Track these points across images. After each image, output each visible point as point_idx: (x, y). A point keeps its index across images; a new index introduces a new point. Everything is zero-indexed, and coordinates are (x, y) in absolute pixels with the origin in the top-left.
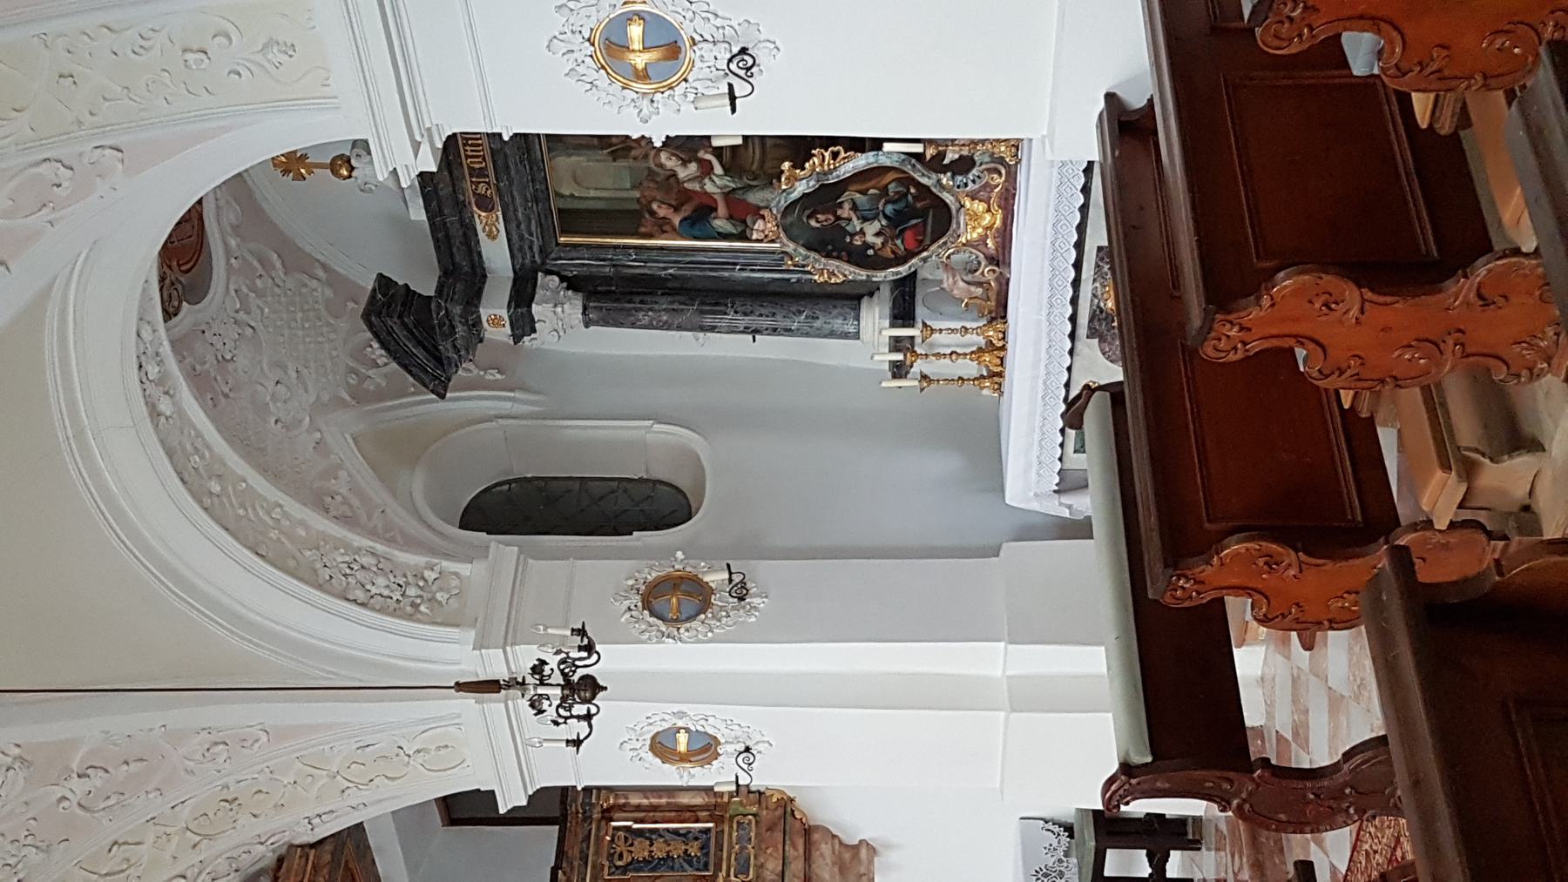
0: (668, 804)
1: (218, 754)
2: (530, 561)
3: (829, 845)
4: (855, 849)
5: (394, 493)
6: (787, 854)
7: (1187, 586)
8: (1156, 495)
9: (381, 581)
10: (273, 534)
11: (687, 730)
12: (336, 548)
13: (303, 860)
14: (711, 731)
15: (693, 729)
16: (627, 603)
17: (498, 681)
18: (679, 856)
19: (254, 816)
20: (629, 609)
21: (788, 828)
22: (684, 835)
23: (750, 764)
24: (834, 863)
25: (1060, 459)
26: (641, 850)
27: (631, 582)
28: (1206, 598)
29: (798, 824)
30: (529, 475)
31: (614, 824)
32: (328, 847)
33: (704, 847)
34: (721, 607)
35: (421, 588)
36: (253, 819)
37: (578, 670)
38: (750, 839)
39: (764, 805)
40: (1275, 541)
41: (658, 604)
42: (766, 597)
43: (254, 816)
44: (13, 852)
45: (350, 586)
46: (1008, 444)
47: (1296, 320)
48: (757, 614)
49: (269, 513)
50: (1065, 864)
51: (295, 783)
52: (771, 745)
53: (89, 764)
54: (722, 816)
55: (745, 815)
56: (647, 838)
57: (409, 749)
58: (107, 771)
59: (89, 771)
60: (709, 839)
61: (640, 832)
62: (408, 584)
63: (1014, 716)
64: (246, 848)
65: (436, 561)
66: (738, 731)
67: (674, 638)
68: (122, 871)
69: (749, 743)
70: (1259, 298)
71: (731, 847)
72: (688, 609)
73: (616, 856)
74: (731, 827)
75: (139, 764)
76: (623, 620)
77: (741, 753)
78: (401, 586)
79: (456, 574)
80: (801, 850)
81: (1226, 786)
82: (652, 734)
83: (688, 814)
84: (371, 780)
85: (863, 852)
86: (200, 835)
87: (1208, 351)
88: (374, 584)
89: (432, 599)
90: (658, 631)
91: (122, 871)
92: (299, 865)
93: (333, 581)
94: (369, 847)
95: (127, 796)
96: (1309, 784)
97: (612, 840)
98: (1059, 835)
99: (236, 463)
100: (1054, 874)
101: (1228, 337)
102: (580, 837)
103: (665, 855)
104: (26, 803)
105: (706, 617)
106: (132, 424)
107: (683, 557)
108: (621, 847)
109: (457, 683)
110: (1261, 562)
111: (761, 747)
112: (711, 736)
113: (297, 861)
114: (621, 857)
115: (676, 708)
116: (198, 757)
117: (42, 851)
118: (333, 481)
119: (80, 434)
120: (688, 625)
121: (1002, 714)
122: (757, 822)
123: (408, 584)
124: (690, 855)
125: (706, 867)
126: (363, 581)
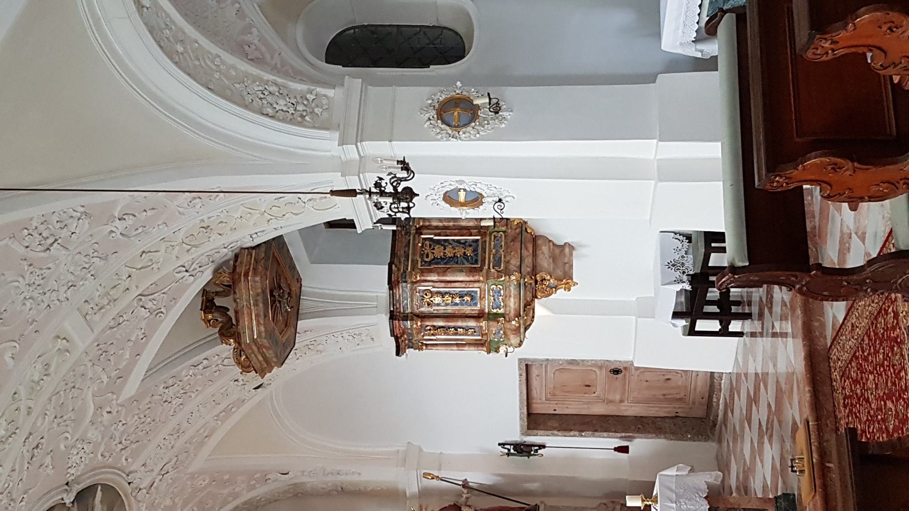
0: (454, 225)
1: (197, 204)
2: (370, 87)
3: (547, 247)
4: (562, 247)
5: (284, 40)
6: (523, 255)
7: (781, 180)
8: (765, 120)
9: (282, 102)
10: (217, 75)
11: (465, 190)
12: (254, 82)
13: (249, 257)
14: (479, 191)
15: (468, 189)
16: (427, 115)
17: (355, 190)
18: (461, 256)
19: (220, 234)
20: (429, 119)
21: (523, 240)
22: (464, 244)
23: (501, 210)
24: (550, 257)
25: (698, 23)
26: (439, 252)
27: (430, 102)
28: (792, 186)
29: (529, 235)
30: (366, 24)
31: (423, 236)
32: (263, 249)
33: (475, 250)
34: (484, 118)
35: (306, 106)
36: (219, 236)
37: (402, 183)
38: (501, 246)
39: (509, 227)
40: (839, 157)
41: (446, 116)
42: (512, 111)
43: (220, 234)
44: (87, 261)
45: (264, 106)
46: (664, 22)
47: (871, 37)
48: (506, 122)
49: (213, 62)
50: (686, 259)
51: (241, 217)
52: (514, 198)
53: (124, 213)
54: (485, 232)
55: (498, 232)
56: (442, 245)
57: (305, 199)
58: (135, 216)
59: (125, 217)
60: (478, 245)
61: (438, 242)
62: (298, 103)
63: (660, 184)
64: (217, 251)
65: (314, 88)
66: (495, 191)
67: (456, 138)
68: (150, 266)
69: (501, 197)
70: (847, 24)
71: (490, 251)
72: (465, 119)
73: (425, 256)
74: (490, 239)
75: (153, 211)
76: (426, 126)
77: (496, 203)
78: (294, 104)
79: (325, 96)
80: (531, 252)
81: (793, 279)
82: (444, 192)
83: (466, 231)
84: (284, 215)
85: (567, 250)
86: (190, 245)
87: (810, 54)
88: (277, 104)
89: (313, 112)
90: (447, 133)
91: (150, 266)
93: (254, 102)
94: (285, 243)
95: (147, 227)
96: (845, 278)
97: (422, 246)
98: (683, 241)
99: (190, 31)
100: (678, 265)
101: (823, 47)
102: (404, 244)
103: (452, 255)
104: (91, 235)
105: (476, 125)
106: (127, 16)
107: (461, 85)
108: (427, 250)
109: (331, 191)
110: (829, 168)
111: (508, 199)
112: (478, 193)
114: (427, 256)
115: (459, 178)
116: (186, 205)
117: (104, 260)
118: (249, 35)
119: (97, 22)
120: (464, 130)
121: (653, 182)
122: (505, 236)
123: (298, 103)
124: (467, 255)
125: (476, 262)
126: (272, 102)
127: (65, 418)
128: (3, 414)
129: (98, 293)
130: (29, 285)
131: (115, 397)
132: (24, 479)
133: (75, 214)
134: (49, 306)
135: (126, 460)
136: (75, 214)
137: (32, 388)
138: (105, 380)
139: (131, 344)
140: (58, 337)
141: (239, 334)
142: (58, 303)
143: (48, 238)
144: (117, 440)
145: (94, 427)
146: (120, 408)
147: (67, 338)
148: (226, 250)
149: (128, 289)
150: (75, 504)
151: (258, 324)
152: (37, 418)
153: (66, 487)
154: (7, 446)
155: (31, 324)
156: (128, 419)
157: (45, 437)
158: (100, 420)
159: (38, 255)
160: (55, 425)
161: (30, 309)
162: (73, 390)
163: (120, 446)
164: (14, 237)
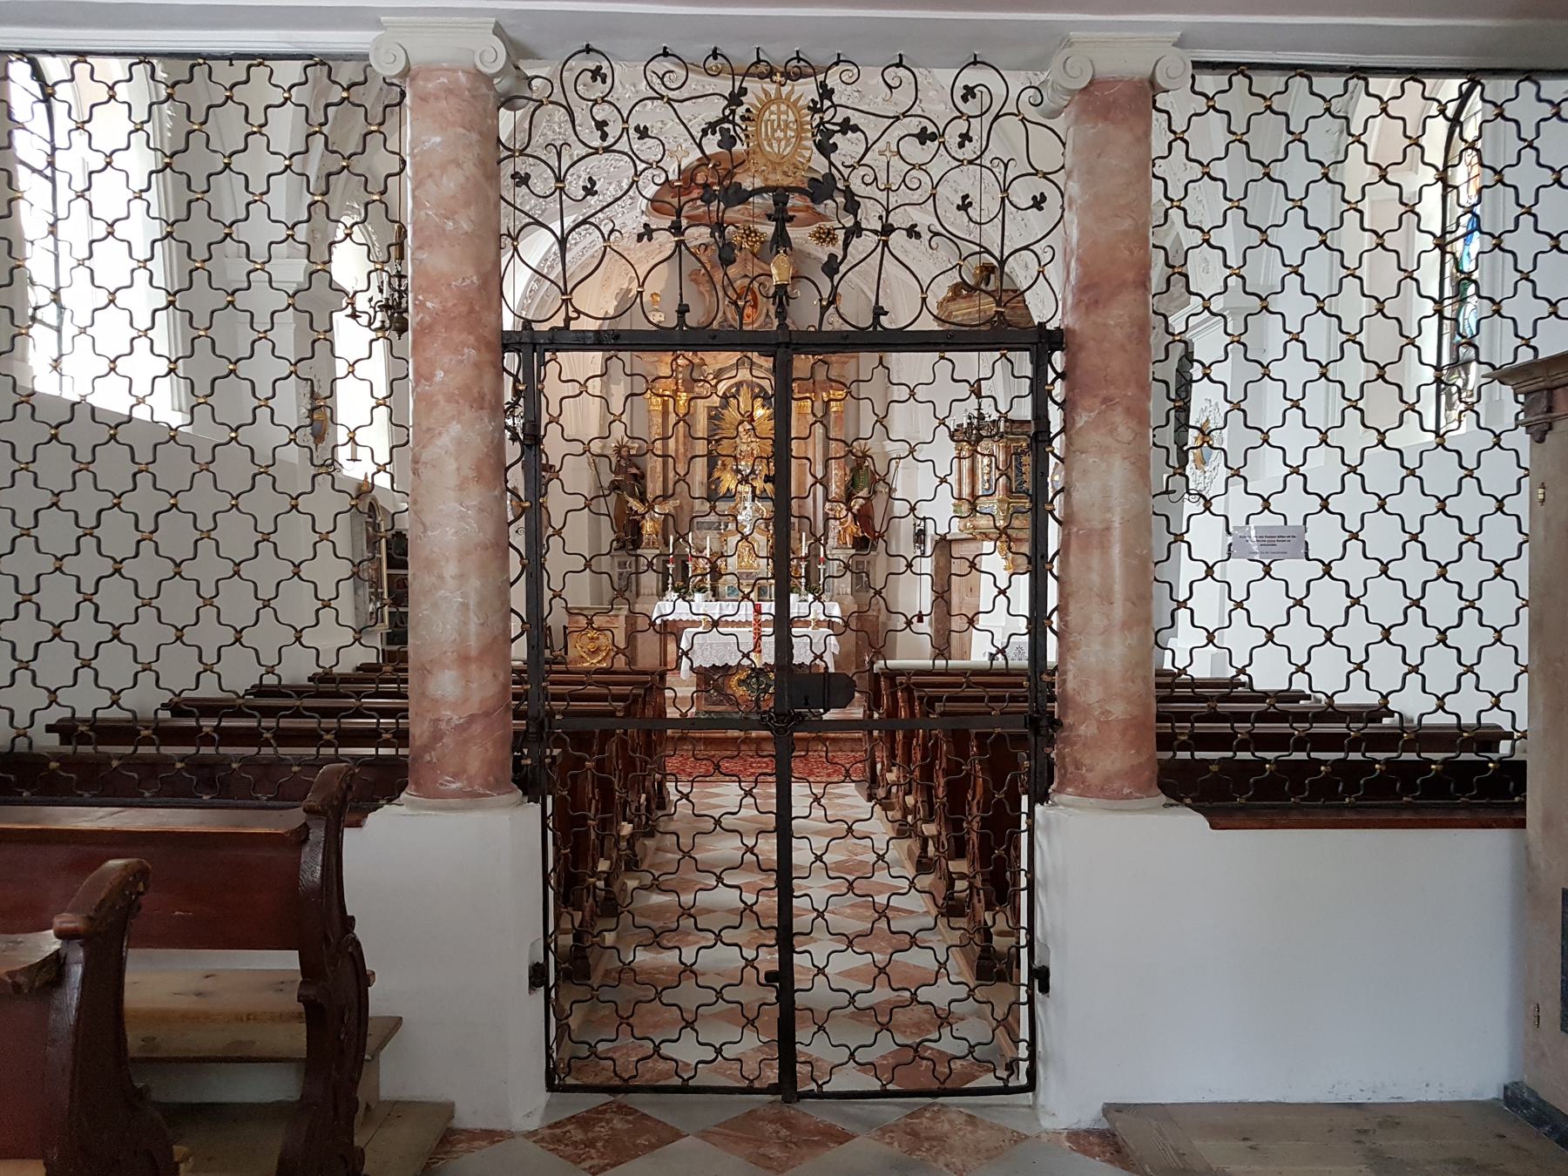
32: (1024, 312)
141: (954, 300)
151: (964, 315)
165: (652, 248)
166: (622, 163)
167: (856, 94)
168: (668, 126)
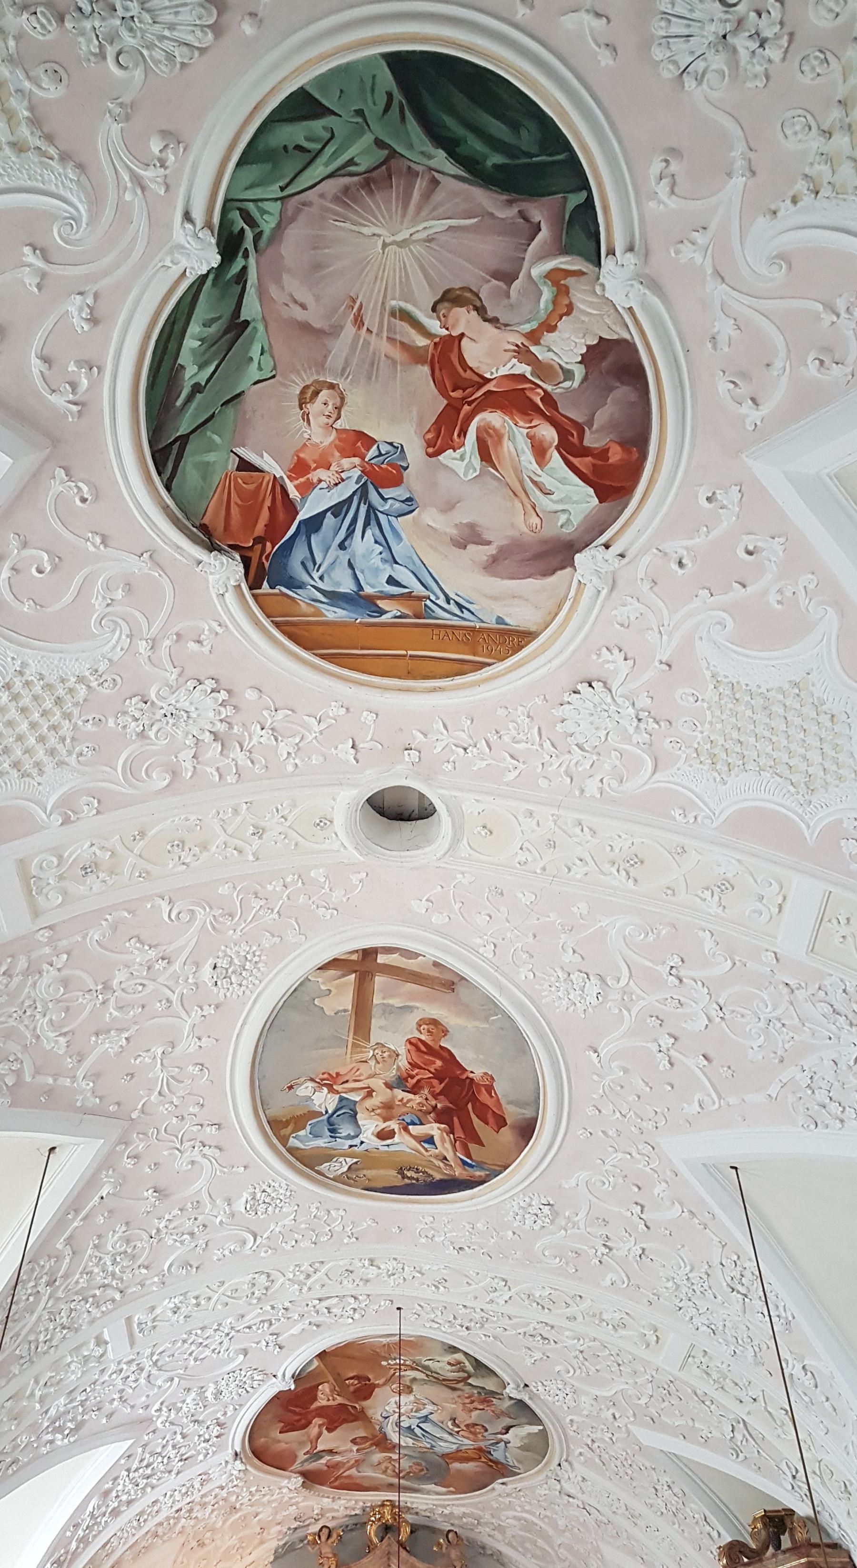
59: (809, 1374)
75: (831, 1409)
92: (835, 1562)
113: (838, 1560)
127: (586, 1363)
128: (555, 1289)
129: (719, 1365)
130: (688, 1279)
131: (632, 1419)
132: (507, 1333)
133: (781, 1309)
134: (680, 1309)
135: (581, 1454)
136: (781, 1309)
137: (594, 1315)
138: (643, 1401)
139: (690, 1423)
140: (656, 1331)
142: (688, 1318)
143: (743, 1285)
144: (593, 1436)
145: (594, 1403)
146: (624, 1429)
147: (660, 1341)
148: (836, 1527)
149: (741, 1402)
150: (513, 1402)
152: (571, 1330)
153: (522, 1386)
154: (527, 1302)
155: (654, 1294)
156: (619, 1445)
157: (557, 1346)
158: (603, 1407)
159: (721, 1280)
160: (573, 1354)
161: (666, 1288)
162: (615, 1364)
163: (590, 1443)
164: (723, 1246)
165: (247, 1532)
166: (207, 1352)
167: (546, 1209)
168: (277, 1285)
